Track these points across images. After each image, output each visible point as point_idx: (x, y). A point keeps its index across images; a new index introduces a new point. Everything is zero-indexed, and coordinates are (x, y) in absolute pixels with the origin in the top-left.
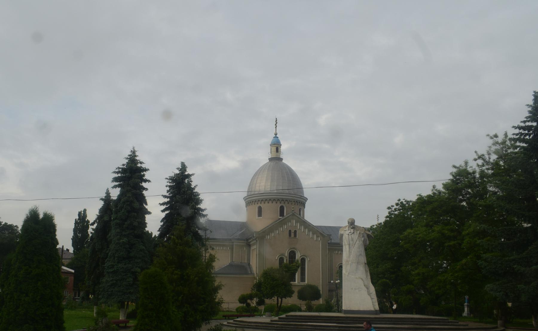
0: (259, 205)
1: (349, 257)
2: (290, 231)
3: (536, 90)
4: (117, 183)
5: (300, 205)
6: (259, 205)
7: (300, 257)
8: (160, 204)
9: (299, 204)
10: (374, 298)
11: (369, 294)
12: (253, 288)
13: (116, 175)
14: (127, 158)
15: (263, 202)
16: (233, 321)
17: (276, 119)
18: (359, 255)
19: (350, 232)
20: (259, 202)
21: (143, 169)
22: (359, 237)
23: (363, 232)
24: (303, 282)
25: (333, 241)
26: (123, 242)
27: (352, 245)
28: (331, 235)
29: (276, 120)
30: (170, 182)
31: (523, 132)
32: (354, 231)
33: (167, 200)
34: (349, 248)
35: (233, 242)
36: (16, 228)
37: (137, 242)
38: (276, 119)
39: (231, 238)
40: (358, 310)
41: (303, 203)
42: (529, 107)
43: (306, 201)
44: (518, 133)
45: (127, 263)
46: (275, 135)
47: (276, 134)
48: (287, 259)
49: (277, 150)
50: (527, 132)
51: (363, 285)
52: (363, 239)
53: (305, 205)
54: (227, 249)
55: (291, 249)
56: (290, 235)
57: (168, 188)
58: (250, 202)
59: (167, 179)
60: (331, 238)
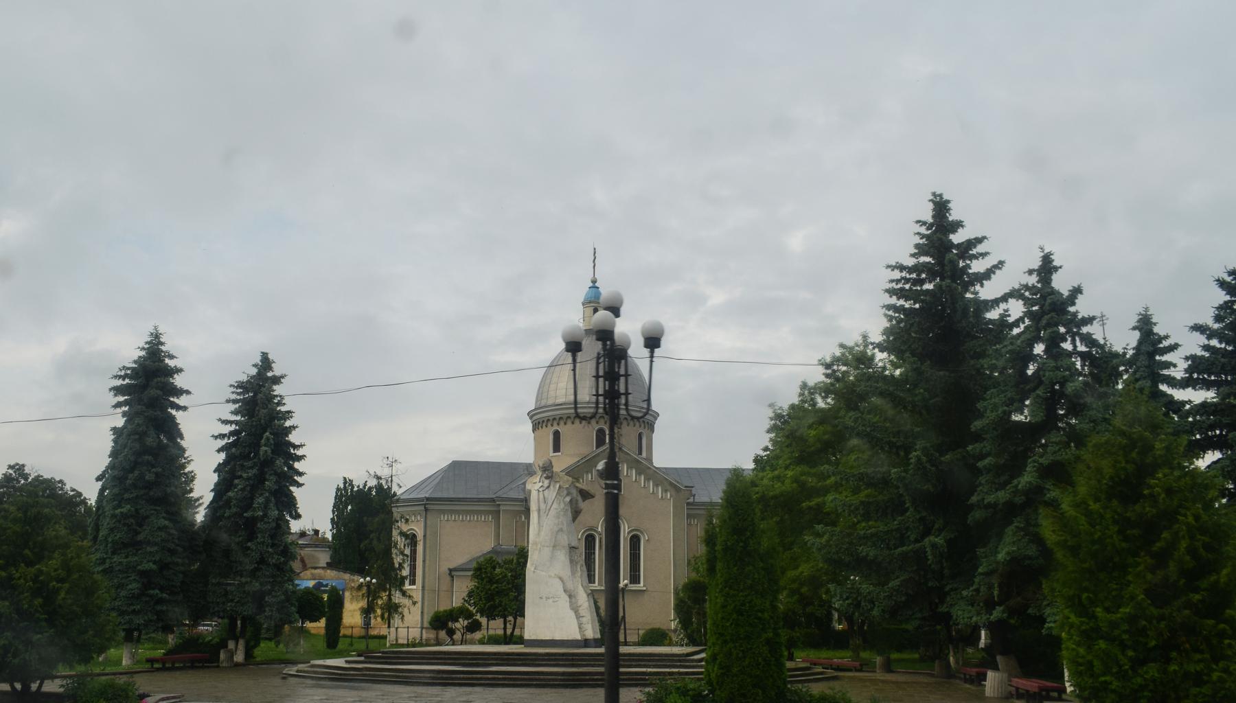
0: (556, 427)
1: (539, 534)
3: (935, 190)
5: (640, 426)
6: (556, 427)
7: (629, 533)
8: (213, 436)
10: (584, 615)
11: (575, 609)
12: (467, 599)
13: (119, 382)
14: (143, 349)
15: (562, 423)
16: (821, 667)
17: (595, 249)
18: (558, 531)
19: (542, 486)
21: (172, 369)
22: (558, 496)
23: (568, 486)
24: (636, 584)
25: (698, 499)
26: (121, 513)
27: (545, 512)
28: (692, 487)
30: (238, 394)
31: (908, 276)
32: (550, 484)
33: (227, 429)
34: (539, 516)
35: (499, 505)
36: (60, 485)
37: (152, 512)
38: (595, 249)
39: (494, 496)
40: (551, 639)
41: (650, 422)
42: (921, 225)
43: (656, 419)
44: (899, 278)
45: (131, 553)
46: (592, 282)
47: (594, 282)
48: (601, 538)
50: (914, 276)
51: (562, 590)
52: (568, 499)
53: (653, 426)
54: (472, 518)
59: (231, 386)
60: (693, 492)
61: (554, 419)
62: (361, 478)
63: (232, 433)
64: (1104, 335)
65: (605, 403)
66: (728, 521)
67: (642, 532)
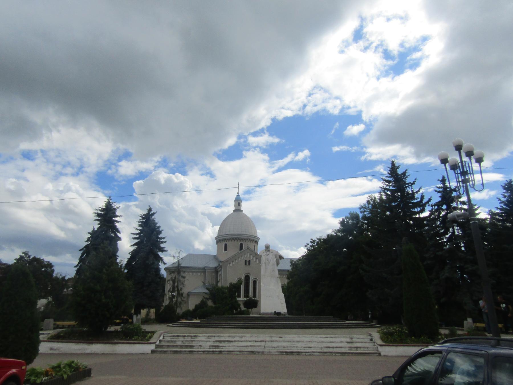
0: (225, 242)
4: (98, 218)
6: (225, 242)
19: (266, 254)
20: (225, 241)
29: (239, 184)
41: (255, 240)
43: (259, 240)
49: (239, 204)
55: (246, 274)
56: (246, 264)
57: (161, 229)
58: (219, 241)
62: (327, 234)
63: (137, 234)
65: (461, 209)
66: (216, 289)
67: (257, 279)
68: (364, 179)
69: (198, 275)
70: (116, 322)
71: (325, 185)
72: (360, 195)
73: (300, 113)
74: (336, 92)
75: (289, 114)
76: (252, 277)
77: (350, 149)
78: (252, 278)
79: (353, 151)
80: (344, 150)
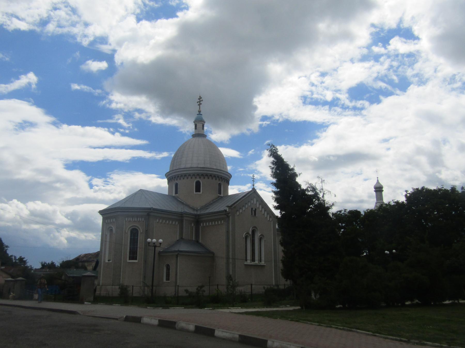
2: (252, 209)
6: (198, 179)
9: (223, 181)
41: (227, 179)
47: (200, 112)
61: (182, 176)
64: (200, 109)
68: (105, 130)
69: (130, 221)
70: (419, 300)
71: (58, 127)
72: (99, 148)
73: (38, 29)
74: (86, 17)
75: (23, 26)
76: (259, 233)
77: (94, 91)
78: (259, 235)
79: (96, 94)
80: (85, 90)
